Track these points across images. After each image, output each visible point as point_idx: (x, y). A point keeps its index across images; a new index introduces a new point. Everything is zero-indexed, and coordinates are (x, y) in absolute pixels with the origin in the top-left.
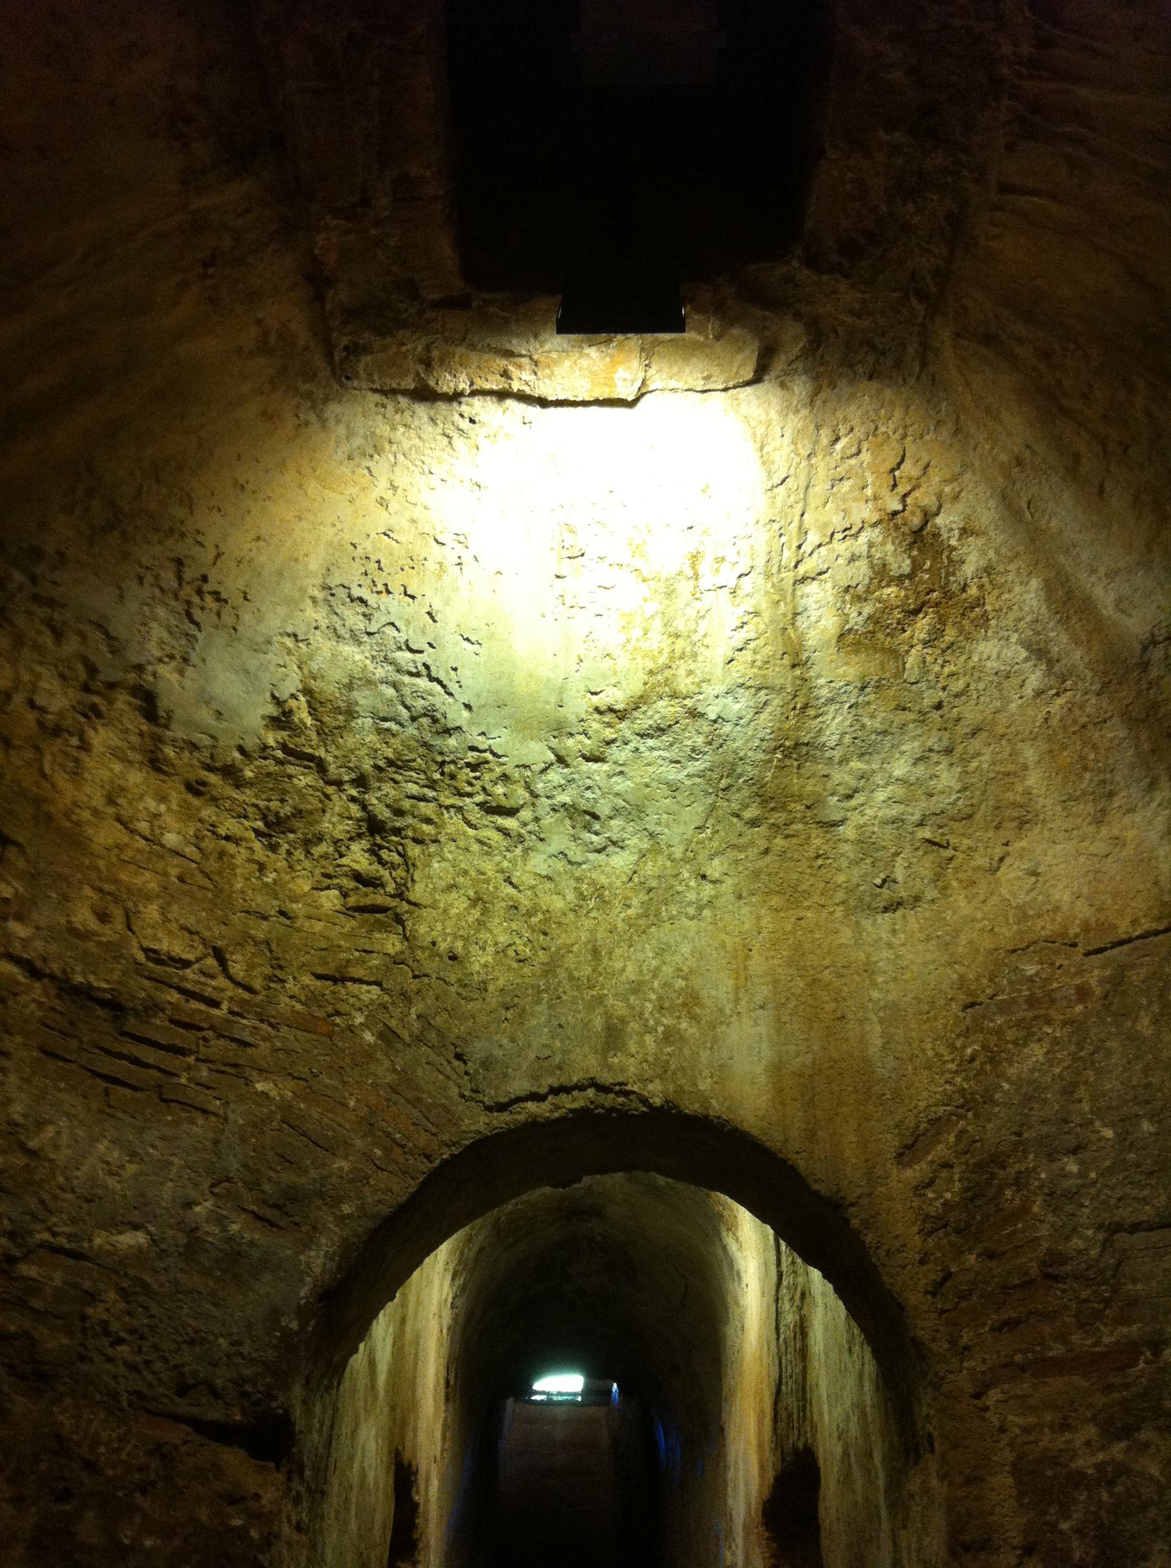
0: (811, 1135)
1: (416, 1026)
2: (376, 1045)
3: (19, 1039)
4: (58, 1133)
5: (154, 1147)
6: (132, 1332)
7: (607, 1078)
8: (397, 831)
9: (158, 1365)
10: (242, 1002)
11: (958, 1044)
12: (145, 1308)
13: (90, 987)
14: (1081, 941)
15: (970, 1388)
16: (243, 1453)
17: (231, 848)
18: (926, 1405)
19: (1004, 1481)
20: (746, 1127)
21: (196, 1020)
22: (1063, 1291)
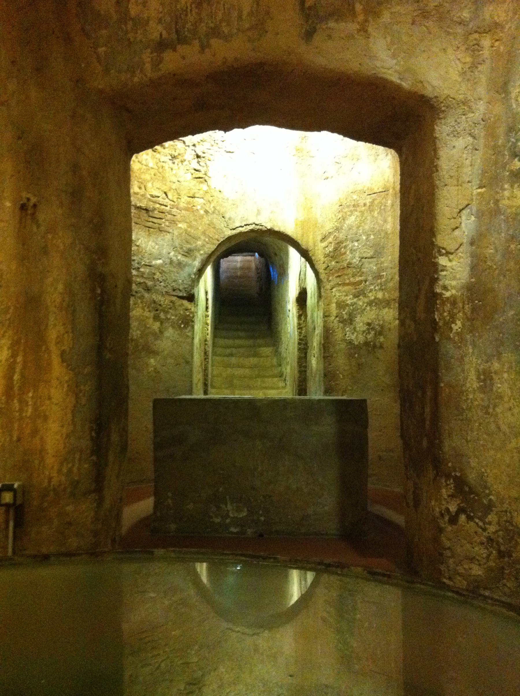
0: (303, 235)
4: (142, 241)
7: (257, 223)
8: (204, 157)
10: (173, 205)
13: (141, 206)
16: (186, 301)
17: (164, 164)
18: (322, 290)
19: (334, 305)
20: (288, 234)
21: (164, 211)
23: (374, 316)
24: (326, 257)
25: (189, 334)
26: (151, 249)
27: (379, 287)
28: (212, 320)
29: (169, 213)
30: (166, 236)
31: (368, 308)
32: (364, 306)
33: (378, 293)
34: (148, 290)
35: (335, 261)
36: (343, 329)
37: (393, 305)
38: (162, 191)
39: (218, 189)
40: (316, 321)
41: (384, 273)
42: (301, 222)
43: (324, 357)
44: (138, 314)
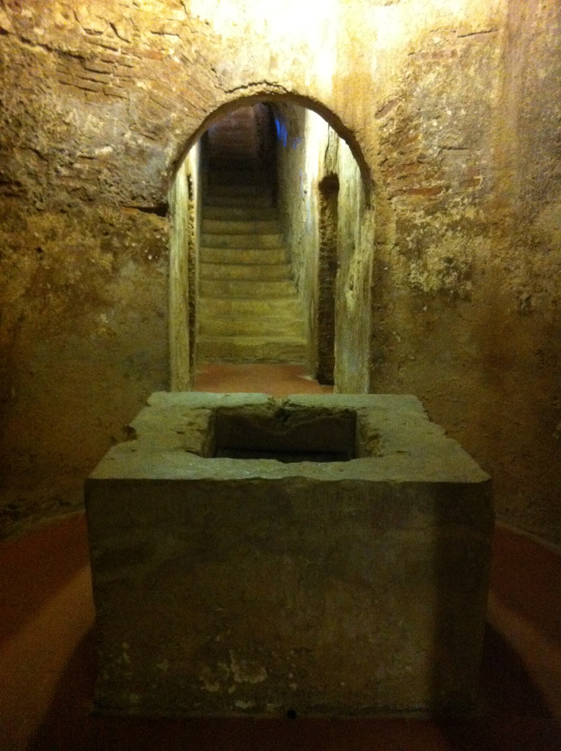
0: (346, 105)
1: (195, 55)
2: (180, 64)
3: (51, 79)
4: (74, 115)
5: (107, 114)
6: (115, 182)
7: (270, 80)
9: (125, 192)
10: (127, 49)
11: (404, 70)
12: (117, 174)
14: (457, 30)
15: (387, 197)
19: (393, 225)
21: (111, 59)
22: (423, 167)
23: (457, 249)
24: (383, 144)
25: (162, 270)
26: (92, 128)
27: (470, 200)
28: (198, 212)
29: (121, 62)
30: (116, 104)
31: (450, 233)
32: (443, 231)
33: (467, 209)
34: (90, 200)
35: (398, 151)
36: (406, 265)
37: (493, 233)
38: (106, 21)
39: (202, 19)
40: (356, 235)
41: (481, 177)
42: (344, 80)
43: (373, 308)
44: (74, 242)
